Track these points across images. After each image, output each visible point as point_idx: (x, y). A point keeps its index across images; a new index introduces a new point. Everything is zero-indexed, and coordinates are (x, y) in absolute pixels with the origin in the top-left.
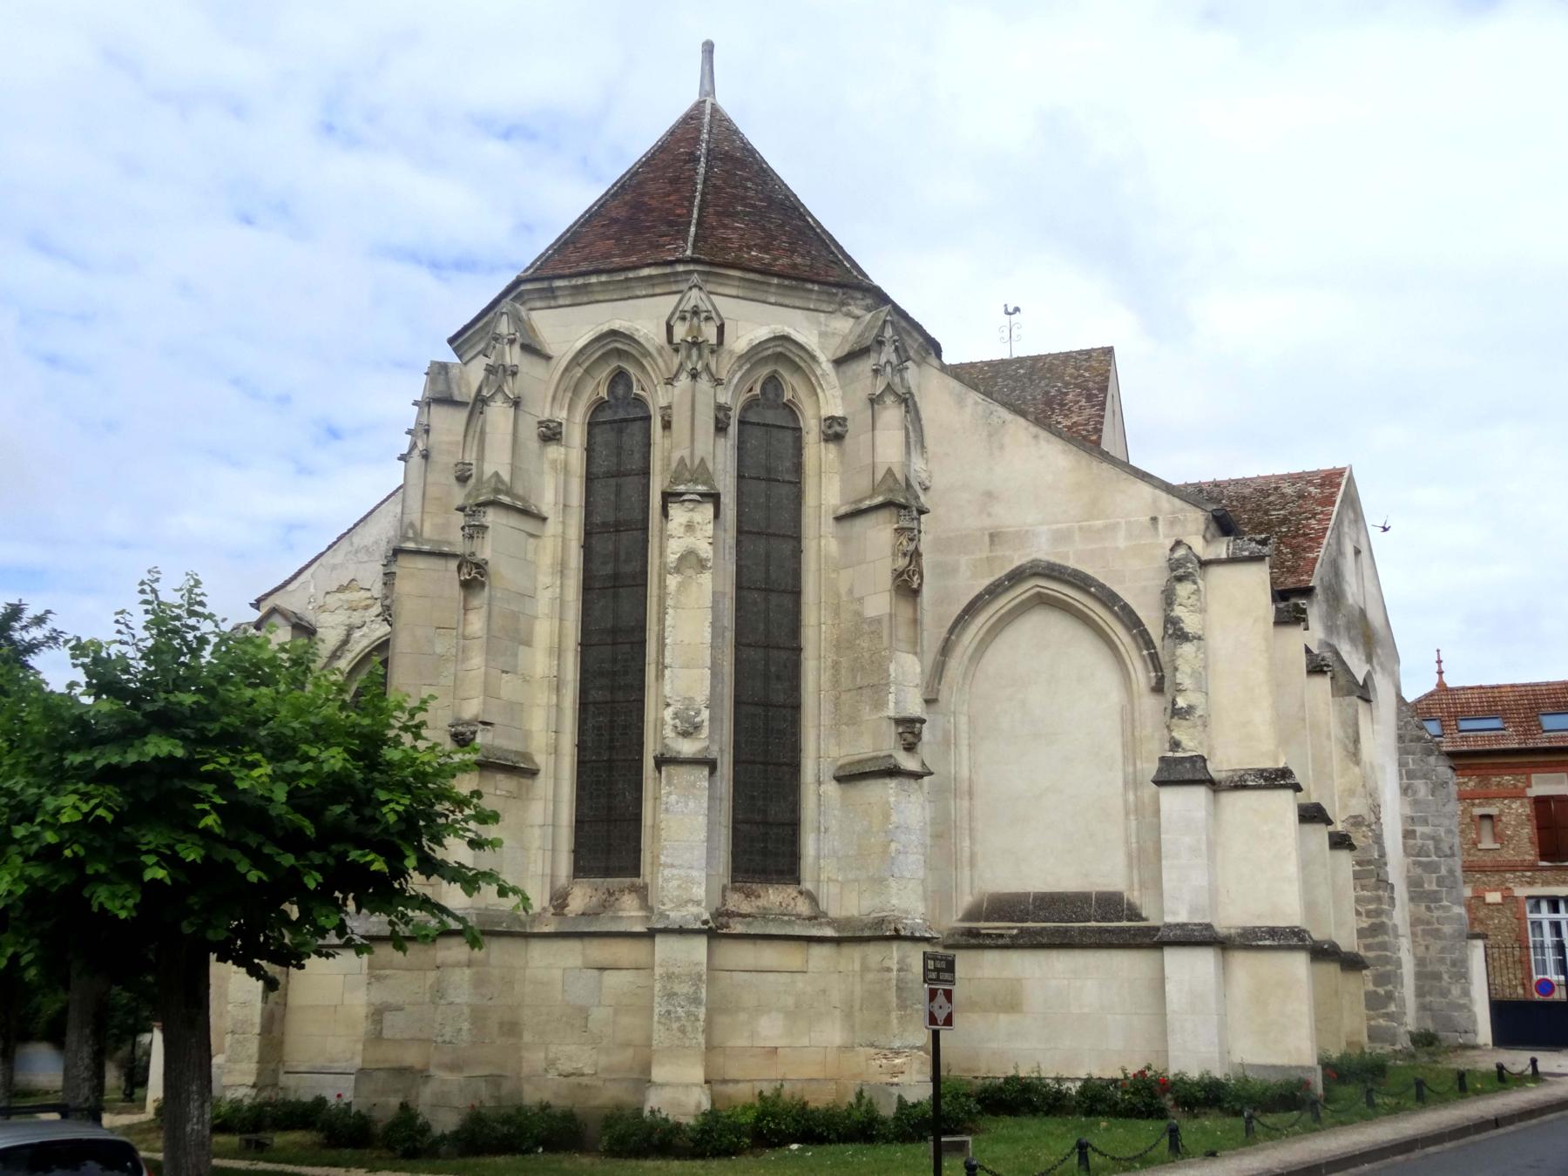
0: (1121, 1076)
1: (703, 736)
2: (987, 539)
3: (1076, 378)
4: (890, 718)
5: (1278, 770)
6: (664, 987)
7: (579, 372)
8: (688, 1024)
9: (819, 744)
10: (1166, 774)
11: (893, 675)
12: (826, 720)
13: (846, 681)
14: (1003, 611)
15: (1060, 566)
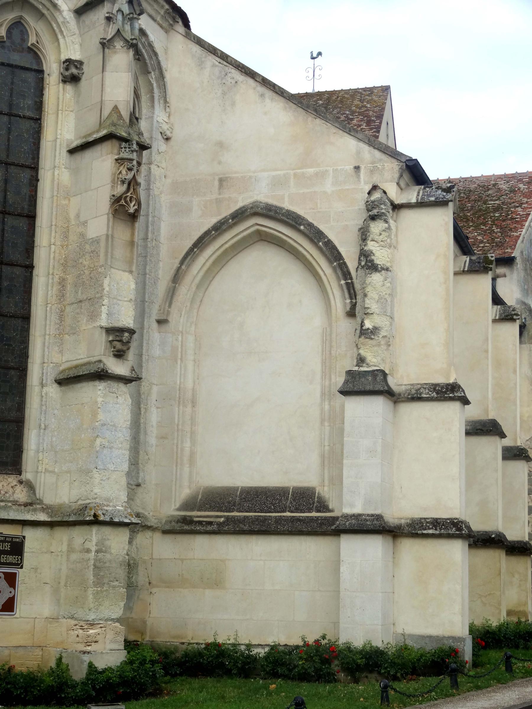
0: (301, 643)
2: (216, 183)
3: (360, 108)
4: (102, 328)
5: (448, 385)
9: (44, 351)
10: (351, 385)
11: (107, 289)
12: (52, 329)
13: (70, 297)
14: (227, 246)
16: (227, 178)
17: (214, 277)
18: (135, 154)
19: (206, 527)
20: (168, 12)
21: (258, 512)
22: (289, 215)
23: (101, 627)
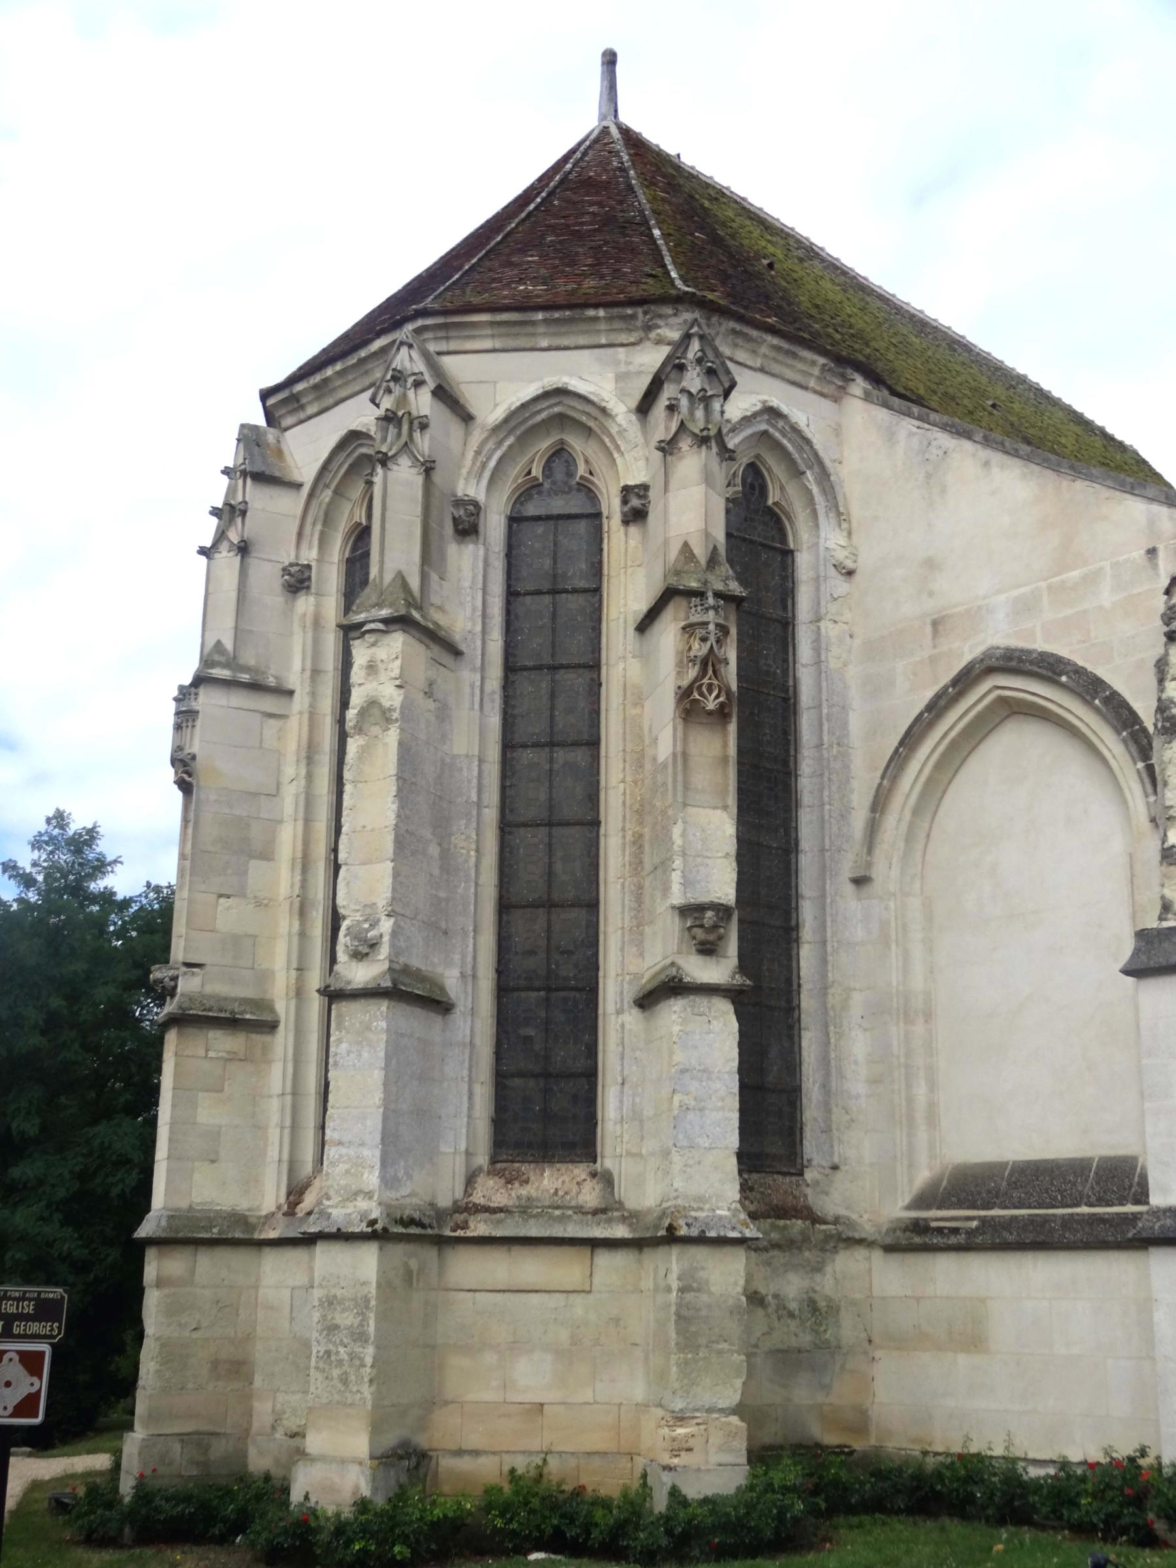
0: (1104, 1460)
1: (381, 957)
2: (928, 629)
6: (324, 1317)
7: (326, 496)
8: (351, 1371)
10: (1144, 958)
11: (678, 841)
14: (953, 734)
15: (1022, 651)
16: (943, 617)
17: (944, 792)
18: (711, 613)
19: (948, 1238)
20: (827, 368)
21: (1035, 1208)
22: (1043, 660)
23: (698, 1424)
